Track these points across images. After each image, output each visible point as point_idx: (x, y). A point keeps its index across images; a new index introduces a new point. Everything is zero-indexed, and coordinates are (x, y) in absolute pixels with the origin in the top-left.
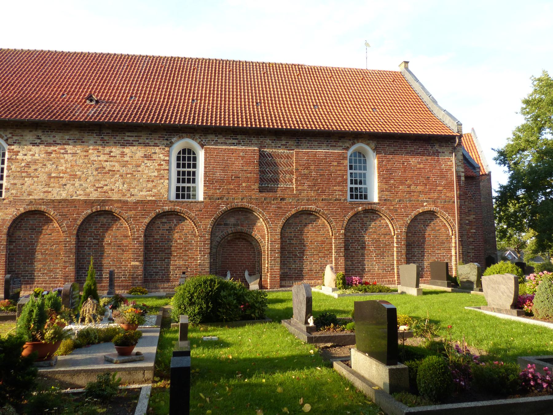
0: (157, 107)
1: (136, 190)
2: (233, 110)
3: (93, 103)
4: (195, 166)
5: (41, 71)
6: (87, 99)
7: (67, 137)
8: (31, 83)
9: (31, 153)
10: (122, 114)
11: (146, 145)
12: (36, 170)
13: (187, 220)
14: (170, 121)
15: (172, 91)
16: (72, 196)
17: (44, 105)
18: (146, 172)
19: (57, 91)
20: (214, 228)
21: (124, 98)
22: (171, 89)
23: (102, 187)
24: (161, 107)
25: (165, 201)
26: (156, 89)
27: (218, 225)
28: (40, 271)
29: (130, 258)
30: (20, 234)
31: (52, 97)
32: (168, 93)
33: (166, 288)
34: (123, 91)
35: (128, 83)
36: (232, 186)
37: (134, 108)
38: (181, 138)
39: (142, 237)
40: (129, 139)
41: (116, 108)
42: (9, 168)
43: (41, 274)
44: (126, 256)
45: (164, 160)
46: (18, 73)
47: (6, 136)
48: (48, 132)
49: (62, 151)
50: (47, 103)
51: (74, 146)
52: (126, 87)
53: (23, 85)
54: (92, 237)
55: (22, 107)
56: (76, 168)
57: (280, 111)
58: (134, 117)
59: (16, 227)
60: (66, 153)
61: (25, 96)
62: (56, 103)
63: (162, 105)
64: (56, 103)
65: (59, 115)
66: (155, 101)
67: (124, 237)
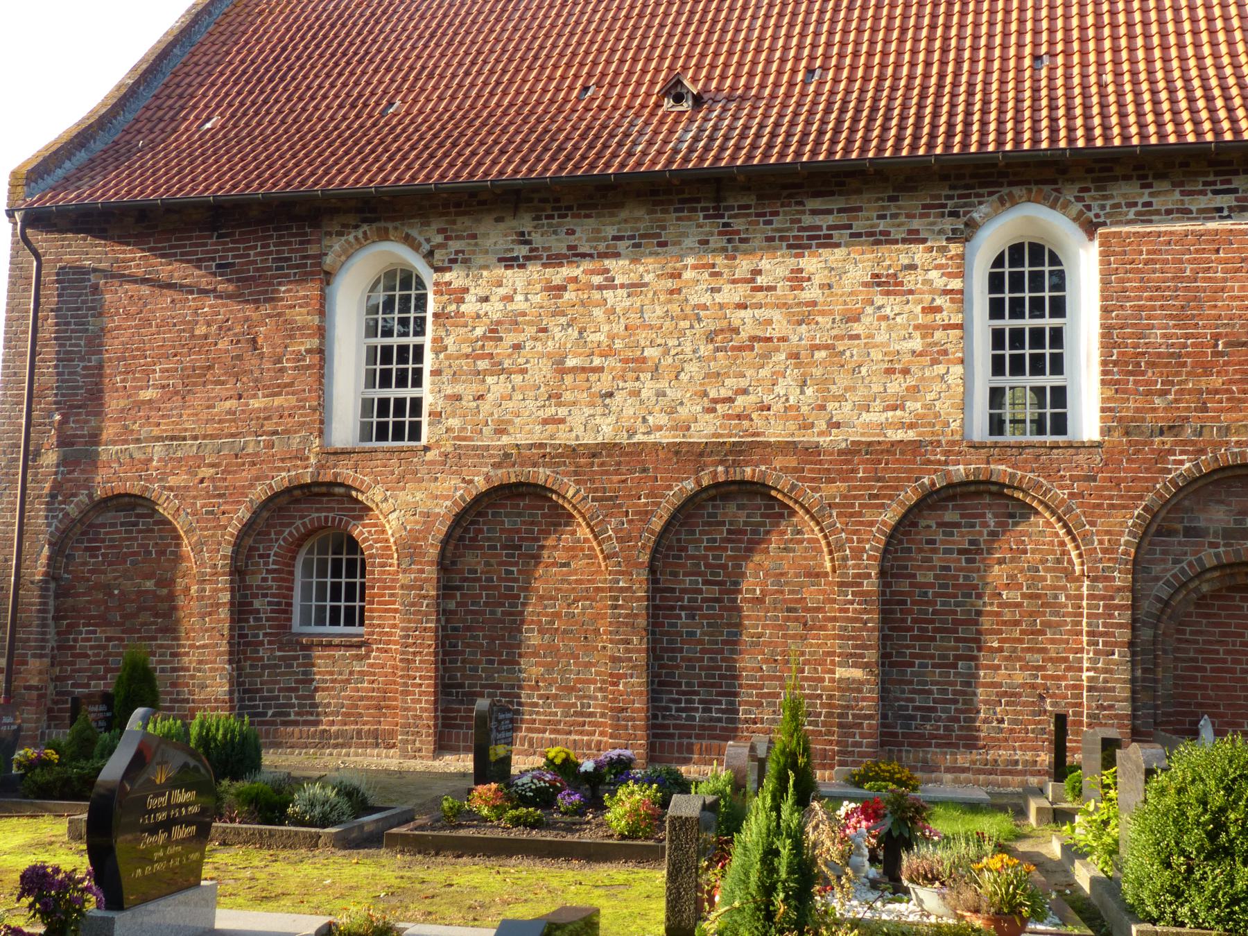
0: (906, 98)
1: (847, 406)
2: (1204, 79)
3: (686, 105)
4: (1059, 308)
5: (509, 19)
6: (665, 93)
7: (611, 231)
8: (485, 62)
9: (502, 291)
10: (789, 135)
11: (880, 239)
12: (517, 347)
13: (1037, 513)
14: (965, 144)
15: (954, 31)
16: (631, 433)
17: (531, 131)
18: (881, 337)
19: (563, 78)
20: (1145, 544)
21: (786, 78)
22: (947, 27)
23: (730, 400)
24: (923, 96)
25: (954, 443)
26: (895, 34)
27: (1159, 533)
28: (537, 687)
29: (833, 654)
30: (473, 561)
31: (552, 101)
32: (938, 44)
33: (964, 770)
34: (778, 54)
35: (791, 25)
36: (1217, 381)
37: (827, 111)
38: (1008, 202)
39: (874, 580)
40: (818, 220)
41: (766, 116)
42: (439, 348)
43: (540, 697)
44: (818, 643)
45: (946, 292)
46: (444, 34)
47: (428, 241)
48: (551, 217)
49: (597, 280)
50: (539, 121)
51: (635, 261)
52: (789, 36)
53: (461, 72)
54: (699, 574)
55: (468, 144)
56: (643, 336)
57: (1211, 72)
58: (834, 142)
59: (461, 539)
60: (610, 284)
61: (472, 107)
62: (567, 120)
63: (924, 88)
64: (567, 120)
65: (584, 157)
66: (896, 78)
67: (808, 575)
